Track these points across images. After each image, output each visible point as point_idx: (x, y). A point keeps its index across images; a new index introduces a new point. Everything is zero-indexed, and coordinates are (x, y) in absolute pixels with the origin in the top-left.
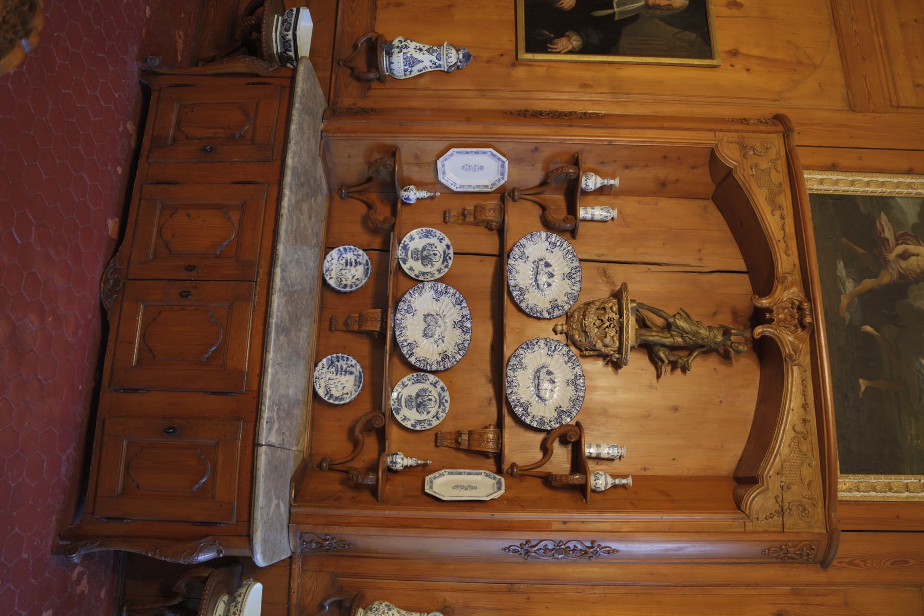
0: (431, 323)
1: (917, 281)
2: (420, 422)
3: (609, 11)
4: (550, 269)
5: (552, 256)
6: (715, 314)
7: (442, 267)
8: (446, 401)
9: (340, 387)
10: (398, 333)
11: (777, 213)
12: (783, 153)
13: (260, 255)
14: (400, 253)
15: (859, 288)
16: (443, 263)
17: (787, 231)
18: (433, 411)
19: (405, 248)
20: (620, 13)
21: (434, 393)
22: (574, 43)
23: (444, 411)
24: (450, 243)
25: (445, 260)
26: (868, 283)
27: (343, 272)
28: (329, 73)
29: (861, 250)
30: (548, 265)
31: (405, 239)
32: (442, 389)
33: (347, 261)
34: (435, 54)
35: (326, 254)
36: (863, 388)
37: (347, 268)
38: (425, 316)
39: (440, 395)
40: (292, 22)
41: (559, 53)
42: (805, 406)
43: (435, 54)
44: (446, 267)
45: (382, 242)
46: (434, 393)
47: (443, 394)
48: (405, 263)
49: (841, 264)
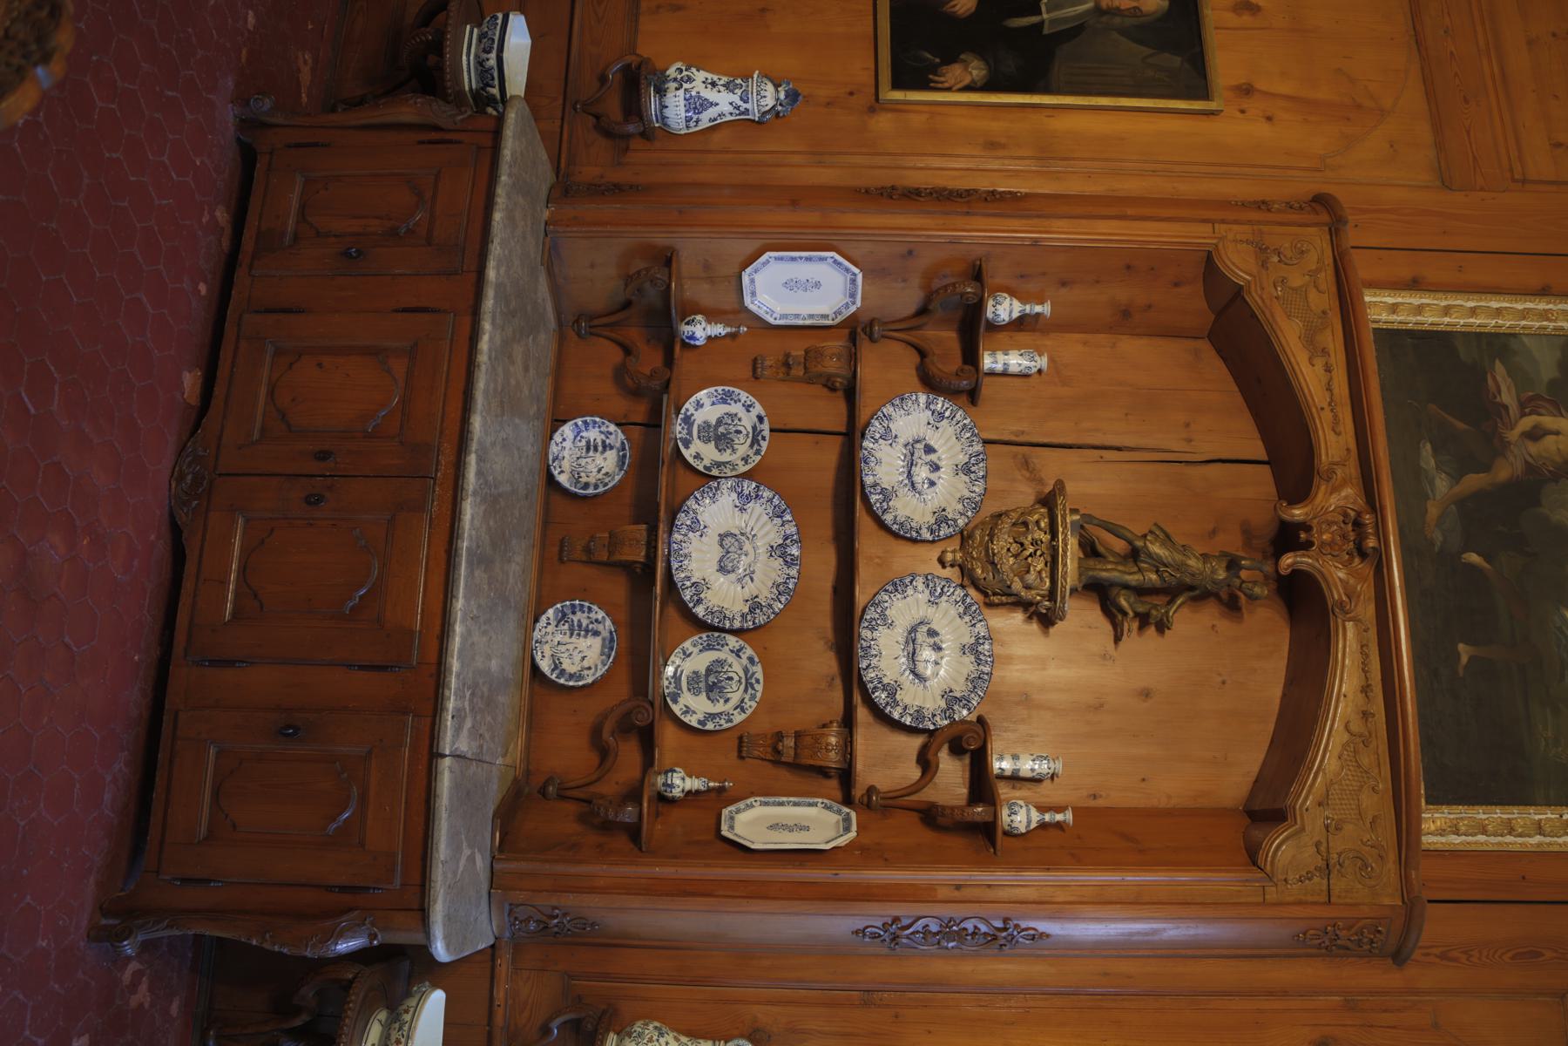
0: (732, 549)
1: (1555, 477)
2: (712, 716)
3: (1034, 19)
4: (933, 457)
5: (937, 435)
6: (1214, 532)
7: (751, 453)
8: (758, 681)
9: (577, 658)
10: (675, 565)
11: (1319, 363)
12: (1329, 260)
13: (441, 433)
14: (679, 429)
15: (1457, 489)
16: (751, 446)
17: (1336, 391)
18: (735, 698)
19: (688, 420)
20: (1053, 22)
21: (737, 667)
22: (975, 72)
23: (753, 698)
24: (763, 413)
25: (755, 441)
26: (1474, 481)
27: (583, 462)
28: (558, 123)
29: (1461, 426)
30: (929, 450)
31: (687, 405)
32: (751, 660)
33: (588, 442)
34: (739, 92)
35: (554, 431)
36: (1464, 659)
37: (589, 454)
38: (722, 537)
39: (746, 670)
40: (496, 38)
41: (949, 89)
42: (1366, 689)
43: (739, 92)
44: (757, 453)
45: (648, 414)
46: (737, 667)
47: (753, 669)
48: (687, 447)
49: (1427, 450)
